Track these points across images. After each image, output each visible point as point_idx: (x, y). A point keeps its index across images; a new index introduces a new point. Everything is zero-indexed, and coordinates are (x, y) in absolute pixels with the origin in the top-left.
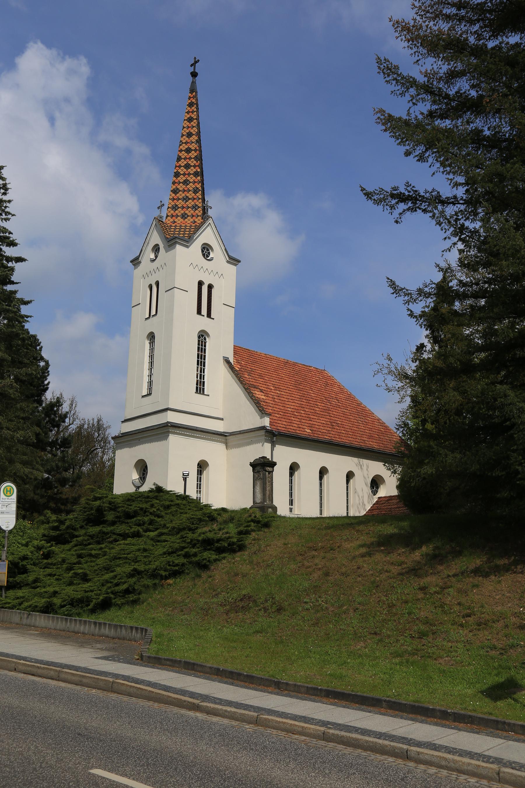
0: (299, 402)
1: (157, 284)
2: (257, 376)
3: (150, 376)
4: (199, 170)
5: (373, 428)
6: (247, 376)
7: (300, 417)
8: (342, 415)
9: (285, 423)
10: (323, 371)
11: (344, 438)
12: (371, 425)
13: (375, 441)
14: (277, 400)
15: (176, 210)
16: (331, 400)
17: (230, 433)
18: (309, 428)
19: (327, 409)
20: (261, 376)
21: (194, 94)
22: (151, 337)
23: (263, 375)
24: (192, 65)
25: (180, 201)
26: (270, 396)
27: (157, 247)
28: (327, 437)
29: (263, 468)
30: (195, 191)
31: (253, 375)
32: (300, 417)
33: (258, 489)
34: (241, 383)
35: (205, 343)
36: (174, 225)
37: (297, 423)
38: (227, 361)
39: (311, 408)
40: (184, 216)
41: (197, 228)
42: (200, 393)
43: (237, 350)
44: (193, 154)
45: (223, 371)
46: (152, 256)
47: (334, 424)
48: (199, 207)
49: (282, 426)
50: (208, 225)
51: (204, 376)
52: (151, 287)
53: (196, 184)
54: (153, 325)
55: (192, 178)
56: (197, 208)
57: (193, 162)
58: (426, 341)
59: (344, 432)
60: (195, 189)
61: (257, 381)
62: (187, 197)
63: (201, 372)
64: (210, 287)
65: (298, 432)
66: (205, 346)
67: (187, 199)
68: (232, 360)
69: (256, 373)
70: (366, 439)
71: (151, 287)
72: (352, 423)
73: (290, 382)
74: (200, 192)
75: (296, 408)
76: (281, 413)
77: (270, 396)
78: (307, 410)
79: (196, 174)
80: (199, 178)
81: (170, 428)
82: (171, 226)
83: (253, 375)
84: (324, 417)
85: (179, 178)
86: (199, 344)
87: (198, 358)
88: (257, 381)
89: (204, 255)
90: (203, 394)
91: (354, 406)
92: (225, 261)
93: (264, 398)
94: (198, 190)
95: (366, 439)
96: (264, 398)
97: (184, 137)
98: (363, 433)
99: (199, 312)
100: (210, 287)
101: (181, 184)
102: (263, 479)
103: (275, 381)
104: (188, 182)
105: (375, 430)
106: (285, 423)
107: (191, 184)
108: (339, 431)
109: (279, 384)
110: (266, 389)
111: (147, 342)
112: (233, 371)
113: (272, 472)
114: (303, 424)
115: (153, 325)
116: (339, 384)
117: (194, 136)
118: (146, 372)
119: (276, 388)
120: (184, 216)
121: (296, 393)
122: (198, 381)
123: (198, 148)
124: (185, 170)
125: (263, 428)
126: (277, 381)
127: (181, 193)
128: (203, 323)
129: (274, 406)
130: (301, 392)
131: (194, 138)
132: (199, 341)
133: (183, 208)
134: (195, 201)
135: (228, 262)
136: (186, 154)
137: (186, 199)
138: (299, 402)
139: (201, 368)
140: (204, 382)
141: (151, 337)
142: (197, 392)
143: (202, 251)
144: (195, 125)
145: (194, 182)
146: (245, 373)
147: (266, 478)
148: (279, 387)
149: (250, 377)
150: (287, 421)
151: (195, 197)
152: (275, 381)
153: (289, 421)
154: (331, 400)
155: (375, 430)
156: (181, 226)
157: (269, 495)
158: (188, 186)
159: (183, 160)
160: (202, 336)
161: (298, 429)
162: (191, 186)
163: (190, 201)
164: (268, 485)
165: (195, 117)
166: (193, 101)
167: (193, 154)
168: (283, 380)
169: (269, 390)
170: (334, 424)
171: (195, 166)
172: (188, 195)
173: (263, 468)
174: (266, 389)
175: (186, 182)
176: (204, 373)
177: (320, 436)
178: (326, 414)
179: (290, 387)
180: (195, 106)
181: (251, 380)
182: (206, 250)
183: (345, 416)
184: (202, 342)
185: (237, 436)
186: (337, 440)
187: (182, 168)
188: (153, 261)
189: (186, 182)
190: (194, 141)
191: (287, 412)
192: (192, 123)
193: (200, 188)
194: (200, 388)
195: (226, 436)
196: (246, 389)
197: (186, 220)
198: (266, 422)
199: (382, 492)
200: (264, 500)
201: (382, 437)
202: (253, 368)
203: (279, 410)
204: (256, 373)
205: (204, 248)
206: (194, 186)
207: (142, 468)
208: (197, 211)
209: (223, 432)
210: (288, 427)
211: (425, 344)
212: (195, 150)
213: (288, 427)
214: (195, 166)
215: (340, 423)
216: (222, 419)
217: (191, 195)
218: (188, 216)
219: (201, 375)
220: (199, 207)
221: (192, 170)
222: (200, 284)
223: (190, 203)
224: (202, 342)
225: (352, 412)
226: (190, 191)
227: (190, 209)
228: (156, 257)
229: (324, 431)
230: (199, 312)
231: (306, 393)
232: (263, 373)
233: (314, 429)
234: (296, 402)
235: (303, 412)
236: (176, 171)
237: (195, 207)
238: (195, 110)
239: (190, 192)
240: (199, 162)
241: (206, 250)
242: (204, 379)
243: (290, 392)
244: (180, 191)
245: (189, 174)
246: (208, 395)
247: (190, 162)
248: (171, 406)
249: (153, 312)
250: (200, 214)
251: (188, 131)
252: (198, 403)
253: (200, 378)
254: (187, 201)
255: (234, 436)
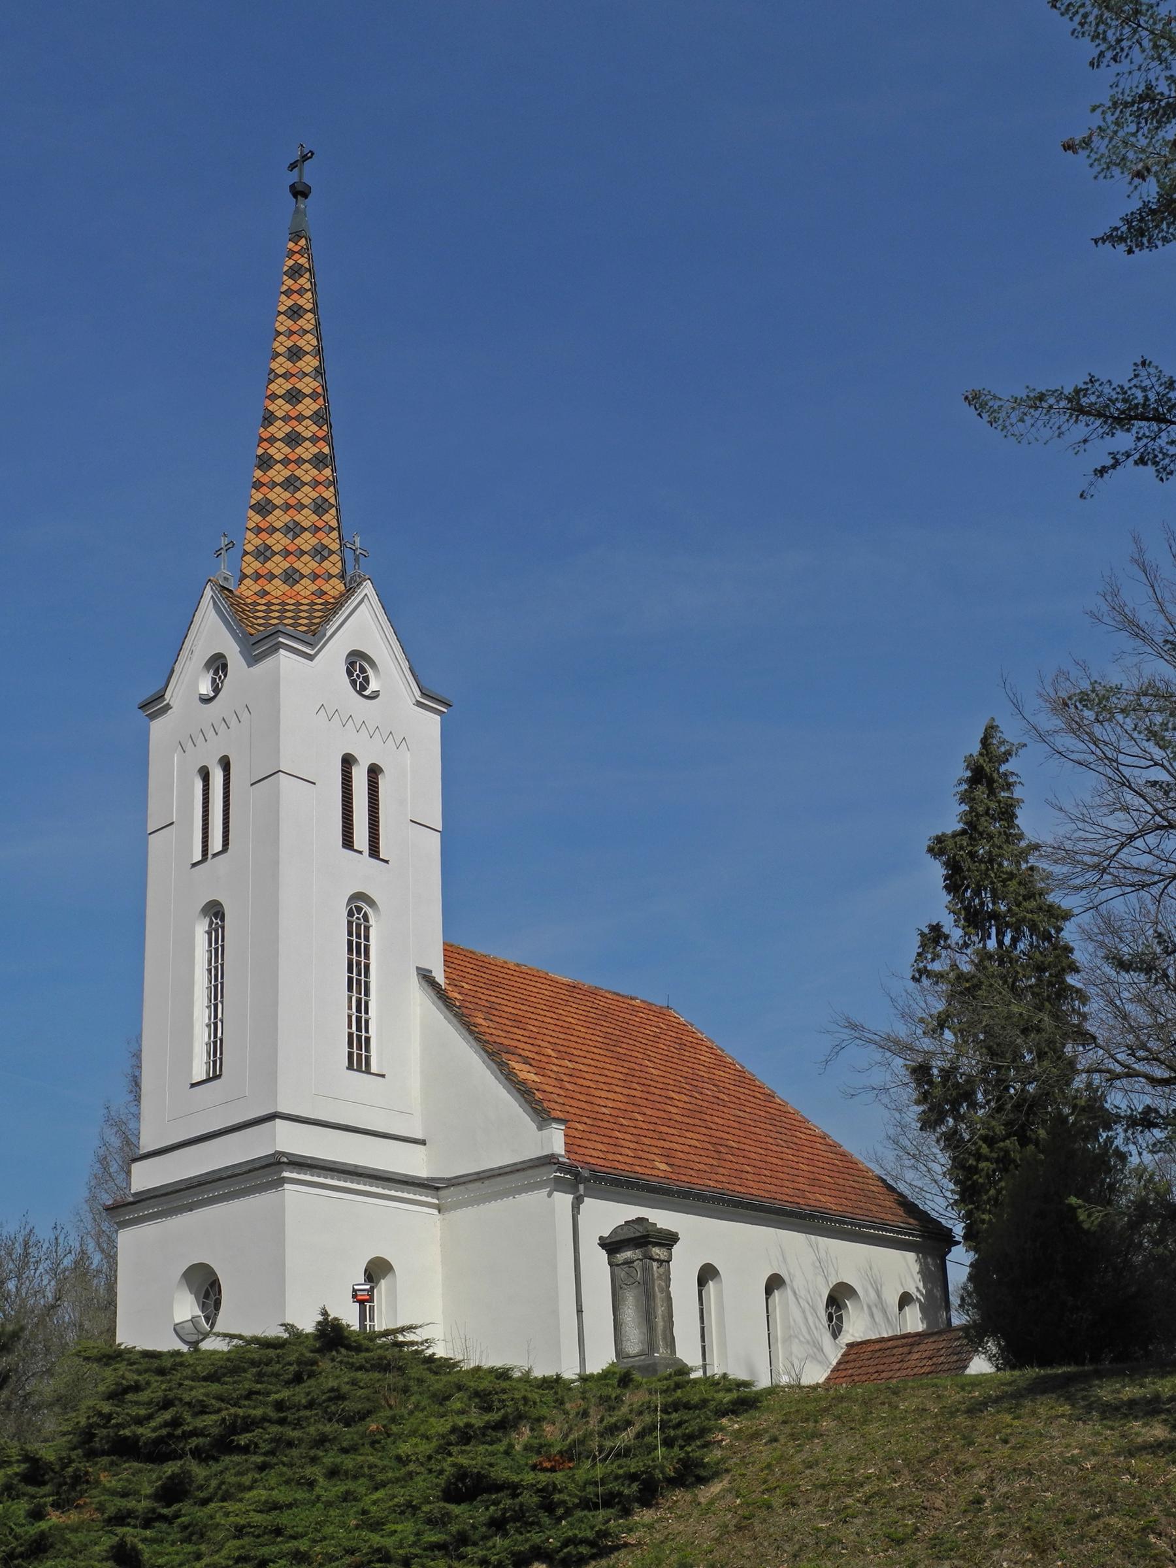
0: (626, 1091)
1: (225, 764)
2: (508, 1022)
3: (215, 1024)
4: (326, 450)
5: (816, 1158)
6: (484, 1023)
7: (635, 1131)
8: (736, 1125)
9: (600, 1146)
10: (664, 1011)
11: (751, 1184)
12: (810, 1150)
13: (827, 1192)
14: (568, 1086)
15: (268, 559)
16: (700, 1084)
17: (449, 1179)
18: (664, 1159)
19: (698, 1109)
20: (517, 1021)
21: (303, 242)
22: (215, 911)
23: (523, 1020)
24: (293, 166)
25: (278, 535)
26: (549, 1073)
27: (219, 663)
28: (711, 1183)
29: (636, 1248)
30: (320, 507)
31: (497, 1019)
32: (635, 1131)
33: (630, 1314)
34: (477, 1039)
35: (367, 929)
36: (264, 601)
37: (632, 1145)
38: (426, 977)
39: (658, 1106)
40: (291, 577)
41: (333, 607)
42: (359, 1070)
43: (451, 953)
44: (308, 407)
45: (420, 1006)
46: (205, 688)
47: (722, 1149)
48: (332, 552)
49: (595, 1154)
50: (362, 601)
51: (367, 1022)
52: (205, 775)
53: (321, 488)
54: (215, 881)
55: (307, 473)
56: (325, 553)
57: (308, 429)
58: (948, 922)
59: (748, 1169)
60: (319, 501)
61: (512, 1036)
62: (297, 524)
63: (359, 1010)
64: (374, 772)
65: (638, 1169)
66: (367, 938)
67: (297, 530)
68: (440, 979)
69: (504, 1015)
70: (807, 1188)
71: (205, 775)
72: (763, 1145)
73: (593, 1038)
74: (333, 511)
75: (620, 1105)
76: (586, 1120)
77: (549, 1073)
78: (649, 1112)
79: (319, 461)
80: (327, 472)
81: (285, 1167)
82: (255, 604)
83: (497, 1019)
84: (693, 1128)
85: (271, 473)
86: (350, 934)
87: (350, 970)
88: (512, 1036)
89: (353, 683)
90: (368, 1071)
91: (758, 1101)
92: (410, 702)
93: (536, 1079)
94: (326, 506)
95: (807, 1188)
96: (536, 1079)
97: (281, 359)
98: (796, 1172)
99: (348, 841)
100: (374, 772)
101: (278, 489)
102: (645, 1283)
103: (553, 1034)
104: (298, 484)
105: (821, 1165)
106: (600, 1146)
107: (306, 489)
108: (737, 1166)
109: (565, 1043)
110: (537, 1057)
111: (201, 928)
112: (447, 1007)
113: (668, 1262)
114: (645, 1148)
115: (215, 881)
116: (709, 1044)
117: (308, 358)
118: (201, 1014)
119: (563, 1054)
120: (291, 577)
121: (612, 1068)
122: (350, 1035)
123: (320, 390)
124: (287, 450)
125: (549, 1160)
126: (561, 1036)
127: (277, 512)
128: (358, 871)
129: (566, 1101)
130: (625, 1064)
131: (309, 363)
132: (350, 923)
133: (286, 553)
134: (320, 534)
135: (419, 704)
136: (288, 407)
137: (294, 530)
138: (626, 1091)
139: (359, 1001)
140: (368, 1039)
141: (215, 911)
142: (350, 1067)
143: (350, 673)
144: (308, 327)
145: (316, 484)
146: (476, 1013)
147: (653, 1280)
148: (569, 1050)
149: (491, 1024)
150: (606, 1140)
151: (320, 524)
152: (553, 1034)
153: (611, 1141)
154: (700, 1084)
155: (821, 1165)
156: (284, 604)
157: (664, 1331)
158: (298, 495)
159: (279, 423)
160: (359, 906)
161: (637, 1162)
162: (306, 495)
163: (306, 535)
164: (659, 1302)
165: (309, 306)
166: (302, 261)
167: (308, 407)
168: (575, 1033)
169: (543, 1059)
170: (722, 1149)
171: (314, 440)
172: (298, 518)
173: (636, 1248)
174: (537, 1057)
175: (292, 484)
176: (367, 1012)
177: (696, 1181)
178: (698, 1122)
179: (596, 1050)
180: (307, 275)
181: (494, 1031)
182: (358, 666)
183: (742, 1127)
184: (359, 926)
185: (470, 1186)
186: (738, 1189)
187: (279, 444)
188: (206, 700)
189: (292, 484)
190: (308, 370)
191: (601, 1116)
192: (301, 322)
193: (332, 501)
194: (359, 1055)
195: (437, 1189)
196: (491, 1055)
197: (297, 587)
198: (555, 1141)
199: (857, 1328)
200: (651, 1344)
201: (841, 1182)
202: (494, 999)
203: (578, 1112)
204: (504, 1015)
205: (352, 664)
206: (314, 495)
207: (206, 1286)
208: (326, 564)
209: (428, 1179)
210: (611, 1156)
211: (946, 930)
212: (314, 396)
213: (611, 1156)
214: (314, 440)
215: (734, 1144)
216: (423, 1142)
217: (307, 518)
218: (303, 576)
219: (359, 1020)
220: (332, 552)
221: (307, 451)
222: (348, 762)
223: (307, 541)
224: (359, 926)
225: (756, 1118)
226: (304, 507)
227: (306, 558)
228: (217, 690)
229: (702, 1167)
230: (348, 841)
231: (637, 1068)
232: (520, 1013)
233: (677, 1162)
234: (618, 1089)
235: (640, 1117)
236: (260, 451)
237: (320, 552)
238: (308, 286)
239: (306, 512)
240: (325, 428)
241: (358, 666)
242: (367, 1031)
243: (598, 1064)
244: (276, 507)
245: (300, 461)
246: (383, 1076)
247: (299, 429)
248: (283, 1109)
249: (216, 844)
250: (335, 571)
251: (289, 344)
252: (356, 1098)
253: (359, 1029)
254: (296, 536)
255: (461, 1188)
